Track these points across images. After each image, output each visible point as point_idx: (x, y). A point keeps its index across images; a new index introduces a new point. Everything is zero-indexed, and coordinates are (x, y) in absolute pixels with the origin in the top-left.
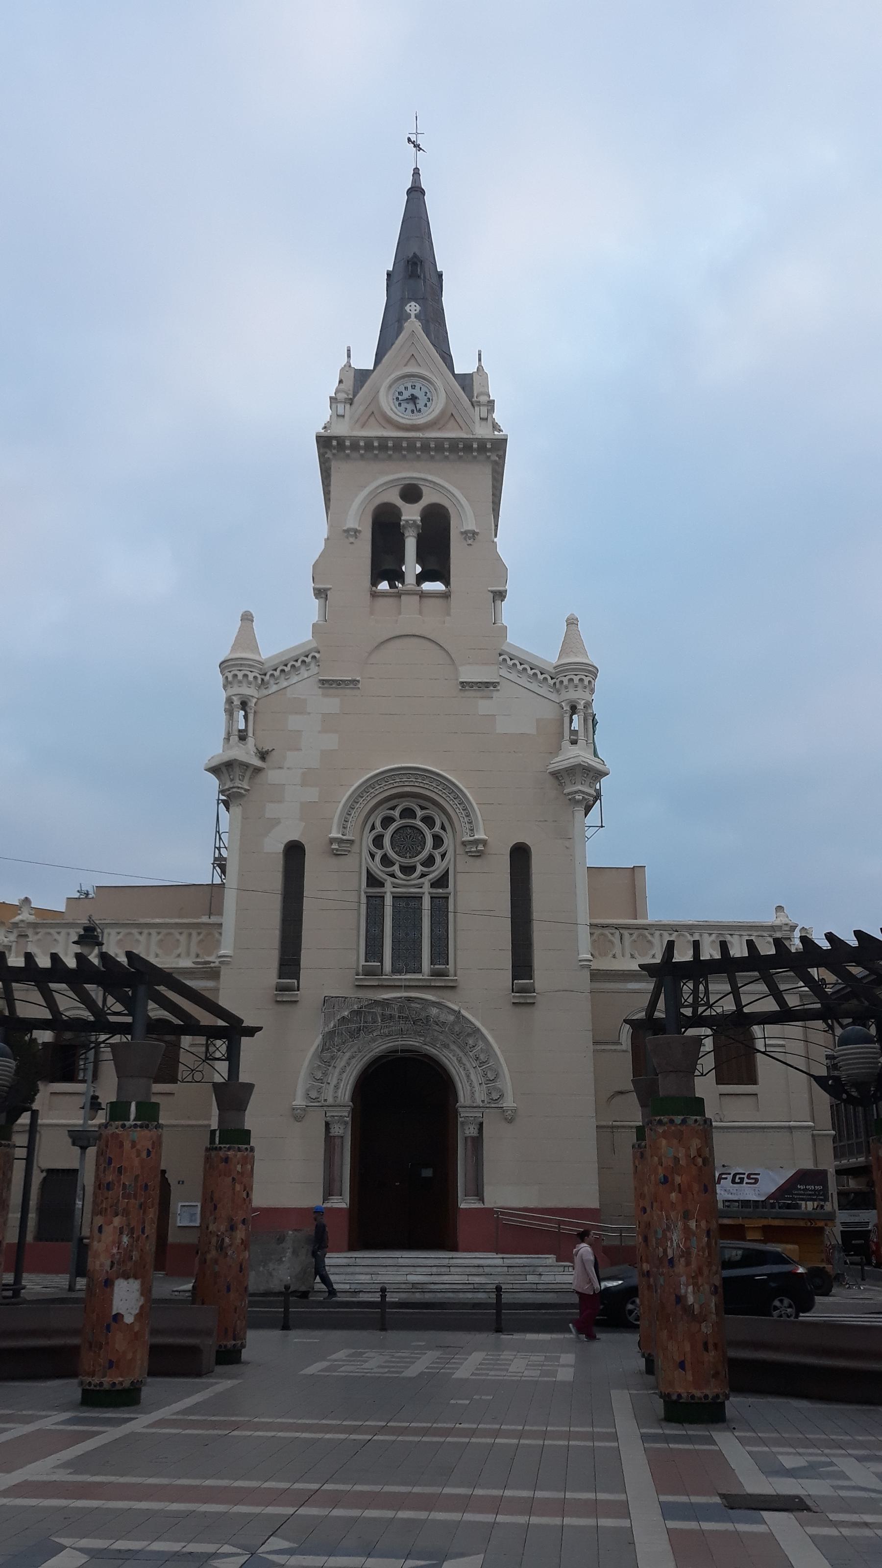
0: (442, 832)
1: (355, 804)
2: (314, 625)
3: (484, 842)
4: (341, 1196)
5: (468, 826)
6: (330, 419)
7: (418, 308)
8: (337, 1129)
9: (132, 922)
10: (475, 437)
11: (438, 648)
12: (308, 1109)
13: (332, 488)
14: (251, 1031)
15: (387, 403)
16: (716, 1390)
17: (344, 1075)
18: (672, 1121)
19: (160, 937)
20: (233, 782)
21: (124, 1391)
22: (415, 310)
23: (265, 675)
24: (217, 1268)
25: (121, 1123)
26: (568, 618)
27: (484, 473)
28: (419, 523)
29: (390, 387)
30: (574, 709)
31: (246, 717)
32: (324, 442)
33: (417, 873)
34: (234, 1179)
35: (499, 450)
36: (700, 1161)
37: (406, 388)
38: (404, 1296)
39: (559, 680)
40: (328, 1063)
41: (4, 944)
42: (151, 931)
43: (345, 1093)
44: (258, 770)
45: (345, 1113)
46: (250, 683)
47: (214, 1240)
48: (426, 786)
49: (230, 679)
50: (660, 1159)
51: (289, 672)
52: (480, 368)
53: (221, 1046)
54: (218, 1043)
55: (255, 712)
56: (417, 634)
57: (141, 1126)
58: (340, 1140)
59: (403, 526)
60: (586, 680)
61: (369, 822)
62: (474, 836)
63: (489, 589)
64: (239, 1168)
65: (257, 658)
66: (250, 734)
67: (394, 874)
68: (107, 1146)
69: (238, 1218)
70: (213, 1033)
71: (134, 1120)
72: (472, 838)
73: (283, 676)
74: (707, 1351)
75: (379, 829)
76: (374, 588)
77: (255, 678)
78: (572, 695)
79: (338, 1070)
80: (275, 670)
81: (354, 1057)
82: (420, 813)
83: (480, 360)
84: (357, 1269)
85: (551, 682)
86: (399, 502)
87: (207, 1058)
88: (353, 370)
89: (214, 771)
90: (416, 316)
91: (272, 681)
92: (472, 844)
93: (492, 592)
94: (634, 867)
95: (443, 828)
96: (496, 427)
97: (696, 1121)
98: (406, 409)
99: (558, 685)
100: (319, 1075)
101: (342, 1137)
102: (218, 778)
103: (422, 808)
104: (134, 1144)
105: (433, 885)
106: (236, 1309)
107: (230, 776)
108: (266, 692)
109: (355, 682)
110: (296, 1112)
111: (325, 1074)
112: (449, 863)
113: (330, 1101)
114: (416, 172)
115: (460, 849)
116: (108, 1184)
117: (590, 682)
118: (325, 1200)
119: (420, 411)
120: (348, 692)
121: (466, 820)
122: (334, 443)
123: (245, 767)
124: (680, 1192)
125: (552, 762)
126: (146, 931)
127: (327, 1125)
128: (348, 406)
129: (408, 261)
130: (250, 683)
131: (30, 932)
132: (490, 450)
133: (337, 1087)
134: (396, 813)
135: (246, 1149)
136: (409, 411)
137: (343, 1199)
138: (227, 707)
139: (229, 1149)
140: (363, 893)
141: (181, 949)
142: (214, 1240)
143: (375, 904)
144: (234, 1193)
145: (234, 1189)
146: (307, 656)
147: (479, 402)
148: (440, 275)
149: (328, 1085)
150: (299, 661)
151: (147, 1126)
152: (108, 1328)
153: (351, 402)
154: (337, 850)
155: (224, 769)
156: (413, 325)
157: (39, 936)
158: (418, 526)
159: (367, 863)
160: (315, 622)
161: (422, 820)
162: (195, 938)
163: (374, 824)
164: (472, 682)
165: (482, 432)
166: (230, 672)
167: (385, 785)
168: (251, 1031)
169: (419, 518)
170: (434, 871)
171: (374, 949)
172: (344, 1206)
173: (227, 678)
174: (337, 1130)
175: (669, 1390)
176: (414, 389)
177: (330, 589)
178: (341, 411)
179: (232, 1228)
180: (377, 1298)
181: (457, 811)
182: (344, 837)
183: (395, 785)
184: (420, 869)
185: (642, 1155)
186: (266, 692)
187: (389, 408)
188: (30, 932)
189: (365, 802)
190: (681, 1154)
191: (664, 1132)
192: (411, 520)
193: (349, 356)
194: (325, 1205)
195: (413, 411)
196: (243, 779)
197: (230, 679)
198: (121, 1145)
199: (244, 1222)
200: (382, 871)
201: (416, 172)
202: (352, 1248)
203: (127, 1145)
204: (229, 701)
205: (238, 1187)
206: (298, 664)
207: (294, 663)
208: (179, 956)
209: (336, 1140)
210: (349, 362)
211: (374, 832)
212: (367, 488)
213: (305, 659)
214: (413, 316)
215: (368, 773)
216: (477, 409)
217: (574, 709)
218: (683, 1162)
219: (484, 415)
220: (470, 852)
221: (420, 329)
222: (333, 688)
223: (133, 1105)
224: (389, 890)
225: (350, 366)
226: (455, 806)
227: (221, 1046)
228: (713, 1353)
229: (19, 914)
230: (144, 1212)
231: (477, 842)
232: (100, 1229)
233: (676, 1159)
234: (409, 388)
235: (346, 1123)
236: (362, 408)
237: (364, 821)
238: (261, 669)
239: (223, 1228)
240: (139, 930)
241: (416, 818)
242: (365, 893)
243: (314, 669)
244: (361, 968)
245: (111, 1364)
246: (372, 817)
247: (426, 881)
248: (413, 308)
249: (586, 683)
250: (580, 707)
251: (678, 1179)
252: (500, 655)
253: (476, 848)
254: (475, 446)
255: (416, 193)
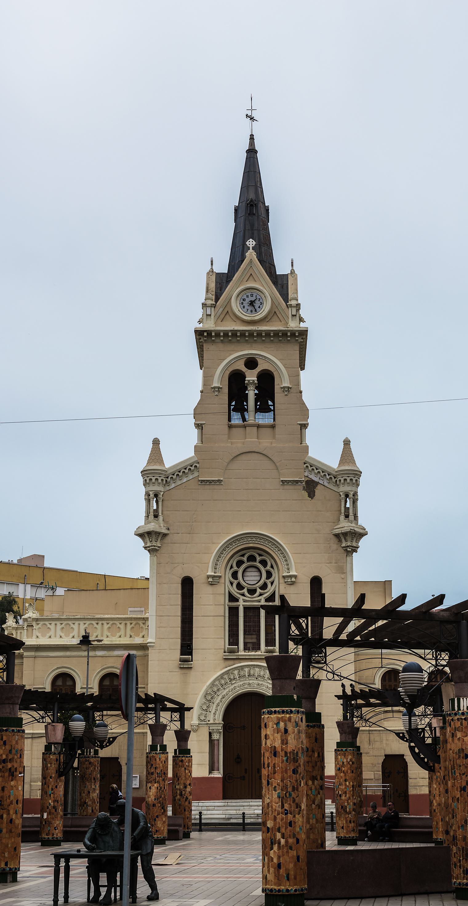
0: (271, 569)
1: (221, 555)
2: (195, 447)
3: (295, 577)
4: (218, 771)
5: (286, 566)
6: (203, 316)
7: (254, 243)
8: (215, 736)
9: (92, 617)
10: (289, 329)
11: (267, 459)
12: (200, 725)
13: (205, 357)
14: (189, 709)
15: (236, 307)
16: (353, 835)
17: (219, 707)
18: (342, 750)
19: (108, 626)
20: (151, 543)
21: (161, 839)
22: (252, 244)
23: (168, 478)
24: (180, 803)
25: (155, 752)
26: (344, 441)
27: (295, 351)
28: (256, 382)
29: (238, 296)
30: (347, 496)
31: (157, 502)
32: (199, 333)
33: (257, 594)
34: (185, 768)
35: (303, 335)
36: (351, 763)
37: (247, 296)
38: (252, 820)
39: (339, 479)
40: (210, 701)
41: (13, 626)
42: (103, 622)
43: (219, 718)
44: (165, 535)
45: (220, 727)
46: (159, 484)
47: (178, 792)
48: (262, 543)
49: (148, 481)
50: (338, 762)
51: (182, 476)
52: (293, 272)
53: (176, 715)
54: (176, 714)
55: (162, 500)
56: (256, 451)
57: (162, 753)
58: (217, 742)
59: (247, 383)
60: (354, 480)
61: (229, 564)
62: (289, 573)
63: (299, 422)
64: (187, 764)
65: (164, 469)
66: (160, 514)
67: (244, 594)
68: (151, 760)
69: (188, 782)
70: (173, 710)
71: (159, 751)
72: (288, 574)
73: (178, 477)
74: (351, 823)
75: (235, 568)
76: (230, 423)
77: (162, 480)
78: (344, 488)
79: (215, 704)
80: (174, 475)
81: (223, 698)
82: (258, 558)
83: (292, 266)
84: (229, 808)
85: (334, 480)
86: (244, 369)
87: (171, 721)
88: (215, 274)
89: (140, 536)
90: (253, 248)
91: (172, 482)
92: (288, 577)
93: (300, 424)
94: (385, 581)
95: (272, 567)
96: (301, 320)
97: (350, 750)
98: (248, 309)
99: (338, 482)
100: (205, 708)
101: (218, 740)
102: (143, 540)
103: (260, 555)
104: (160, 759)
105: (267, 600)
106: (188, 818)
107: (149, 539)
108: (168, 488)
109: (220, 481)
110: (193, 727)
111: (208, 707)
112: (275, 587)
113: (211, 722)
114: (252, 138)
115: (282, 581)
116: (152, 773)
117: (356, 480)
118: (210, 773)
119: (256, 311)
120: (216, 487)
121: (285, 563)
122: (205, 334)
123: (158, 534)
124: (344, 773)
125: (334, 528)
126: (100, 622)
127: (210, 734)
128: (213, 309)
129: (248, 205)
130: (159, 484)
131: (34, 624)
132: (297, 337)
133: (215, 714)
134: (245, 559)
135: (189, 756)
136: (249, 311)
137: (219, 772)
138: (146, 497)
139: (183, 757)
140: (226, 606)
141: (122, 632)
142: (178, 792)
143: (233, 612)
144: (185, 774)
145: (185, 772)
146: (192, 466)
147: (291, 305)
148: (267, 210)
149: (210, 713)
150: (187, 469)
151: (164, 753)
152: (155, 820)
153: (214, 306)
154: (212, 582)
155: (146, 535)
156: (251, 255)
157: (40, 626)
158: (256, 384)
159: (229, 588)
160: (195, 444)
161: (259, 562)
162: (129, 627)
163: (232, 565)
164: (289, 481)
165: (293, 325)
166: (148, 477)
167: (238, 543)
168: (189, 709)
169: (256, 379)
170: (267, 592)
171: (233, 639)
172: (220, 776)
173: (146, 480)
174: (215, 736)
175: (339, 835)
176: (252, 296)
177: (204, 424)
178: (209, 313)
179: (185, 787)
180: (241, 821)
181: (280, 557)
182: (216, 574)
183: (244, 543)
184: (259, 591)
185: (15, 849)
186: (168, 488)
187: (237, 310)
188: (34, 624)
189: (227, 553)
190: (345, 761)
191: (340, 753)
192: (251, 380)
193: (212, 264)
194: (210, 776)
195: (251, 311)
196: (157, 541)
197: (148, 481)
198: (156, 760)
199: (190, 785)
200: (238, 593)
201: (252, 138)
202: (225, 797)
203: (158, 760)
204: (147, 494)
205: (187, 771)
206: (187, 471)
207: (184, 470)
208: (120, 637)
209: (215, 742)
210: (212, 269)
211: (232, 570)
212: (225, 361)
213: (191, 467)
214: (251, 248)
215: (229, 536)
216: (290, 309)
217: (347, 496)
218: (345, 763)
219: (294, 313)
220: (287, 582)
221: (255, 257)
222: (207, 485)
223: (159, 745)
224: (241, 604)
225: (213, 272)
226: (278, 555)
227: (176, 715)
228: (353, 824)
229: (27, 613)
230: (164, 782)
231: (291, 576)
232: (150, 788)
233: (343, 763)
234: (250, 296)
235: (220, 733)
236: (221, 309)
237: (227, 562)
238: (165, 474)
239: (182, 787)
240: (97, 622)
241: (256, 561)
242: (228, 605)
243: (196, 474)
244: (226, 649)
245: (157, 831)
246: (231, 561)
247: (262, 598)
248: (251, 243)
249: (354, 481)
250: (351, 496)
251: (343, 769)
252: (305, 463)
253: (291, 579)
254: (289, 334)
255: (252, 153)
